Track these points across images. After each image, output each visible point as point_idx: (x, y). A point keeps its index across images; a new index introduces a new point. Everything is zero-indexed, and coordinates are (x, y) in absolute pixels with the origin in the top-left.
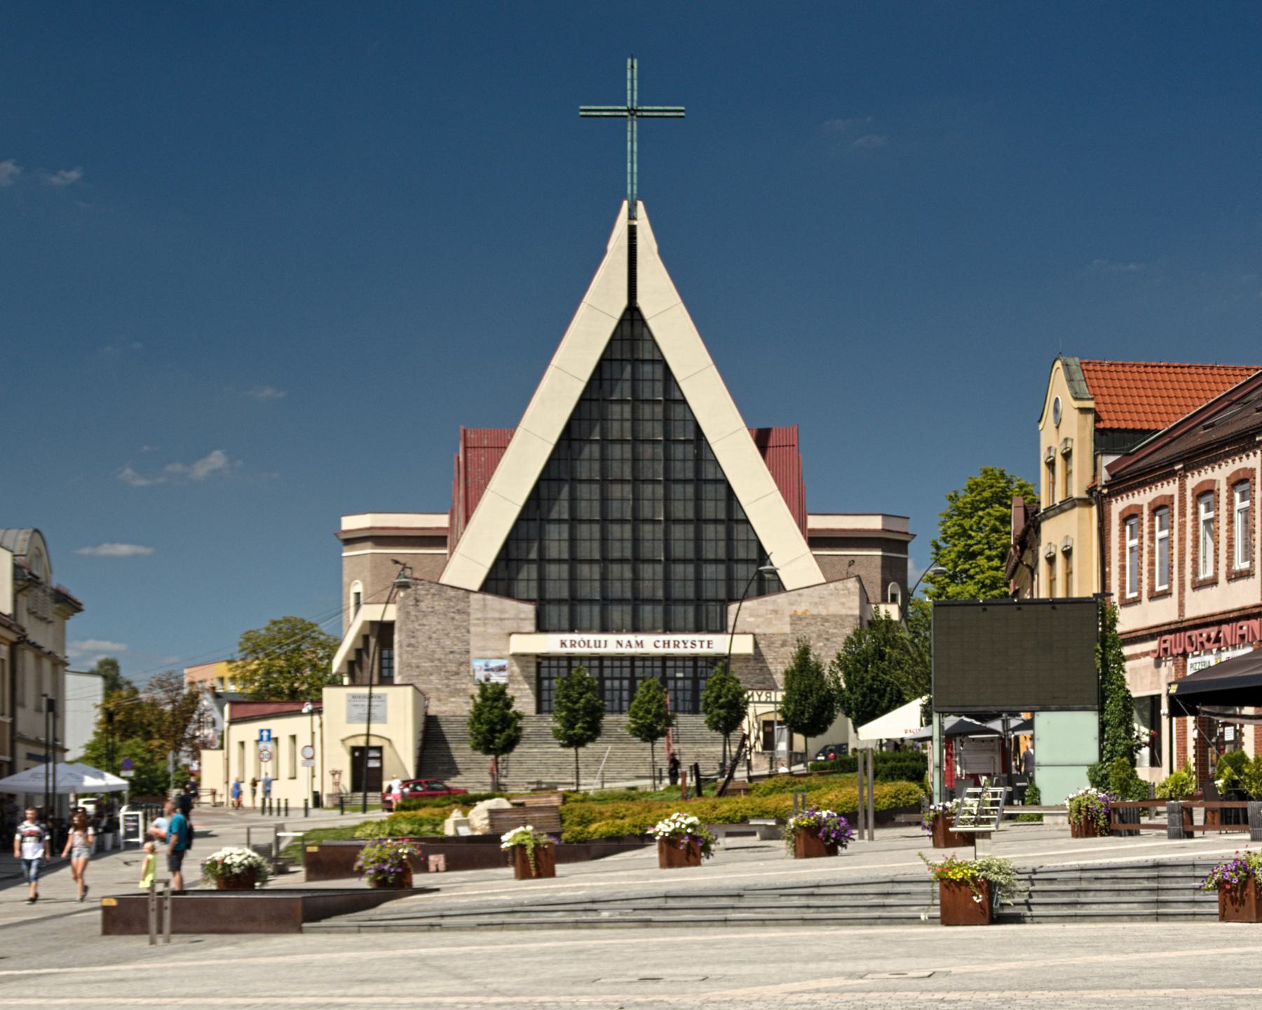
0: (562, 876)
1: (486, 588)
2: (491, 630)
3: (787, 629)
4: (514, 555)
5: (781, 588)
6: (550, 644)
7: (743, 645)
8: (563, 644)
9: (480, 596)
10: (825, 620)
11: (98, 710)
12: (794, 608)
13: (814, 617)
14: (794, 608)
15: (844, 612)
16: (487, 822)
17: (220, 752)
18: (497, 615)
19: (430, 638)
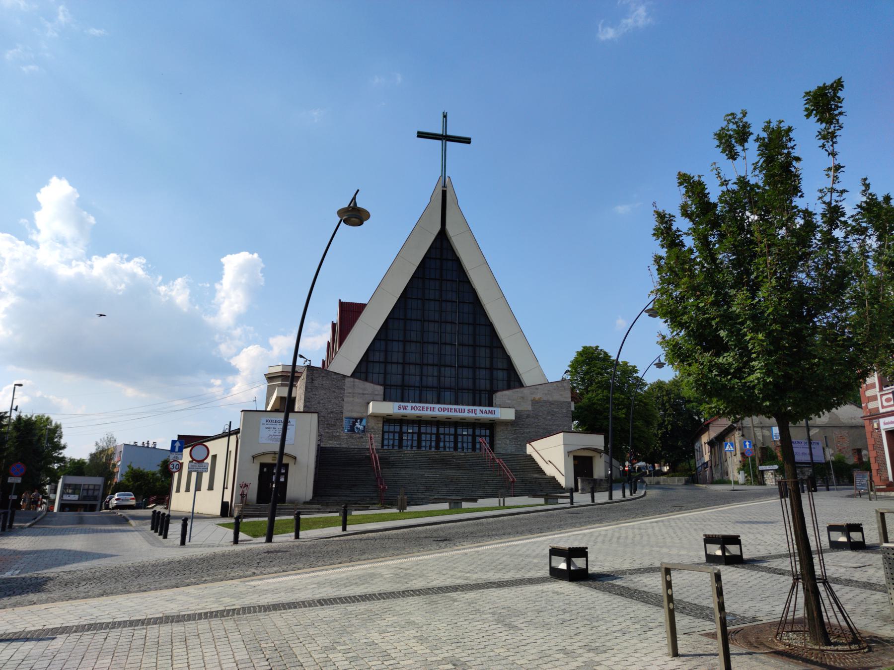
0: (683, 656)
1: (353, 375)
2: (357, 400)
3: (530, 408)
4: (371, 359)
5: (521, 385)
6: (391, 408)
7: (508, 414)
8: (400, 408)
9: (352, 379)
10: (551, 403)
11: (128, 470)
12: (534, 396)
13: (545, 402)
14: (534, 396)
15: (562, 399)
16: (159, 468)
17: (546, 572)
18: (361, 391)
19: (319, 403)
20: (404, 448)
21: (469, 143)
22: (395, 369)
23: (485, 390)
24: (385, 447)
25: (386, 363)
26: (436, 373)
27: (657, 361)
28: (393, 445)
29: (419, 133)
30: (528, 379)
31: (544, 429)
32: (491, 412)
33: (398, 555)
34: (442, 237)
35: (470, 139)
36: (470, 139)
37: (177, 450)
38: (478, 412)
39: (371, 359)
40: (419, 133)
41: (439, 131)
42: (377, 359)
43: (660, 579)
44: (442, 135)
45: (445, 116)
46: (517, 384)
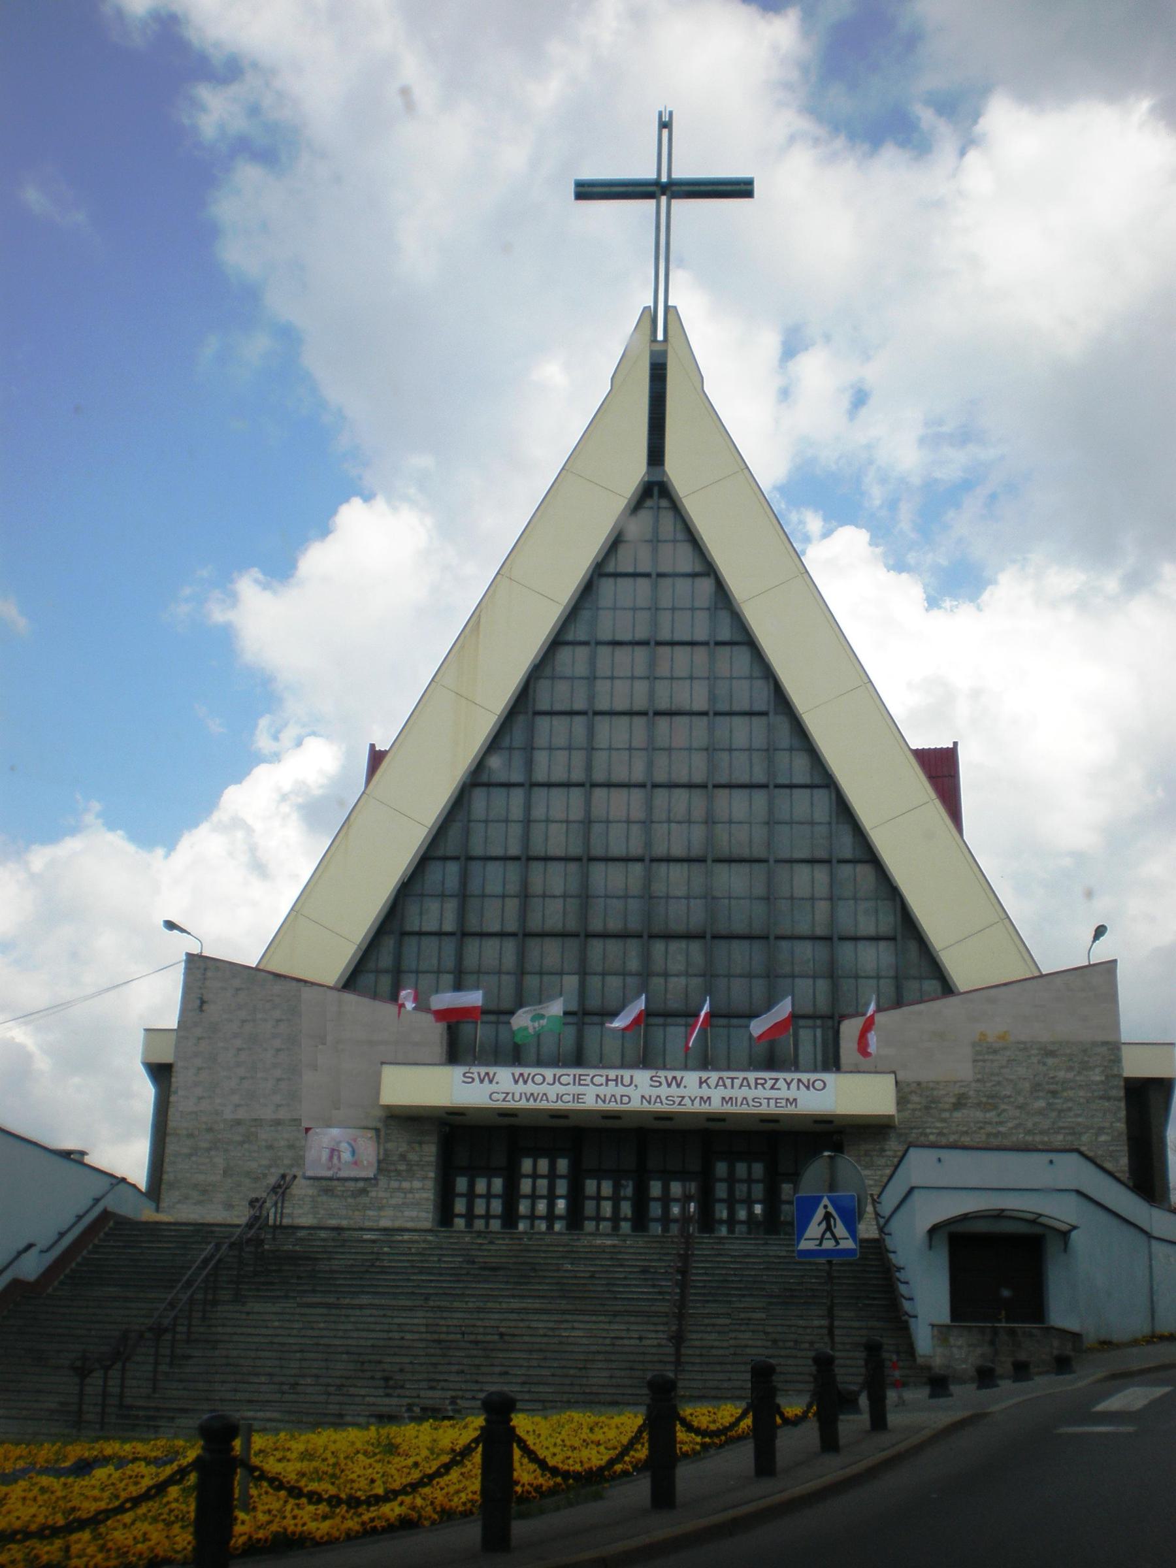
1: (352, 981)
5: (947, 988)
13: (1024, 1047)
20: (589, 1226)
22: (495, 915)
24: (479, 1224)
25: (463, 934)
26: (634, 964)
28: (551, 1217)
29: (579, 185)
30: (965, 967)
33: (534, 700)
34: (655, 492)
35: (749, 183)
36: (749, 183)
39: (413, 924)
41: (647, 172)
42: (431, 925)
43: (430, 1184)
44: (657, 183)
46: (931, 985)
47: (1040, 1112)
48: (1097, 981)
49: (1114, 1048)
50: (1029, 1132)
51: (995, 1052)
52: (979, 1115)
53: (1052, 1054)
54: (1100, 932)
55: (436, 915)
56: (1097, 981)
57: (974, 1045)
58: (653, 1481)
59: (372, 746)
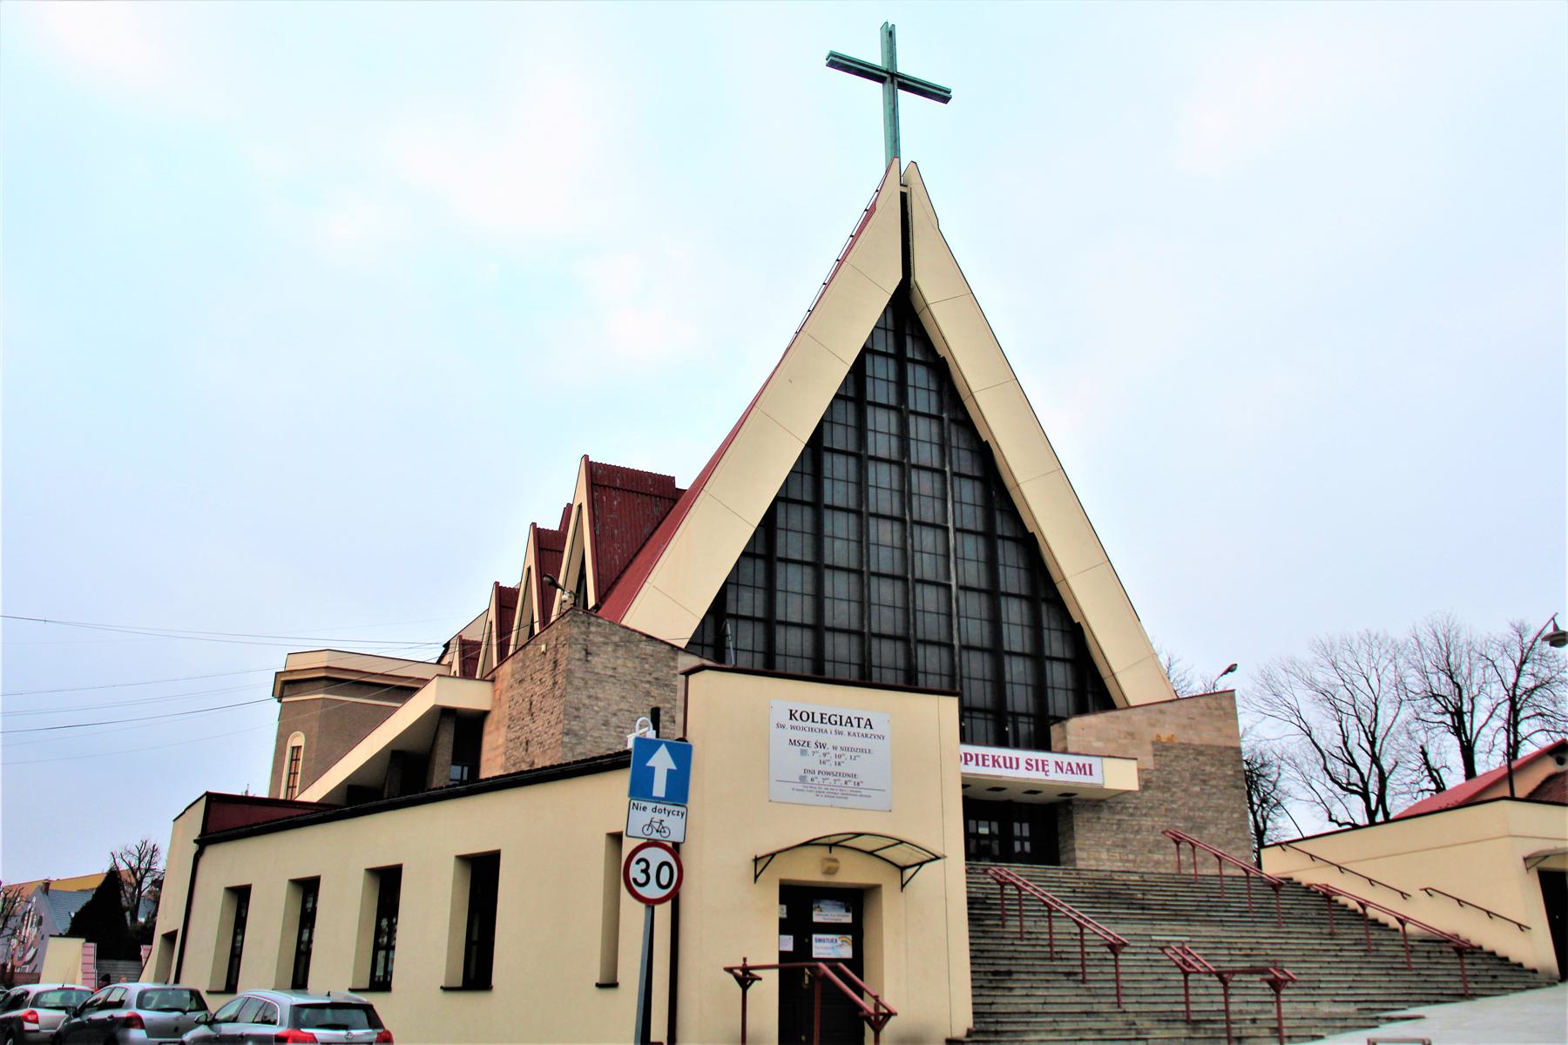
1: (695, 645)
10: (1199, 752)
12: (1157, 731)
13: (1186, 747)
14: (1157, 731)
19: (606, 723)
21: (945, 100)
23: (1026, 715)
27: (1549, 630)
30: (1131, 682)
31: (1186, 819)
32: (1082, 769)
37: (659, 789)
38: (1051, 767)
40: (832, 54)
45: (891, 34)
47: (1197, 795)
48: (1220, 703)
49: (1238, 751)
50: (1191, 809)
51: (1167, 749)
52: (1160, 795)
53: (1201, 753)
54: (1231, 669)
55: (749, 602)
56: (1220, 703)
57: (1153, 743)
58: (650, 756)
59: (534, 524)
